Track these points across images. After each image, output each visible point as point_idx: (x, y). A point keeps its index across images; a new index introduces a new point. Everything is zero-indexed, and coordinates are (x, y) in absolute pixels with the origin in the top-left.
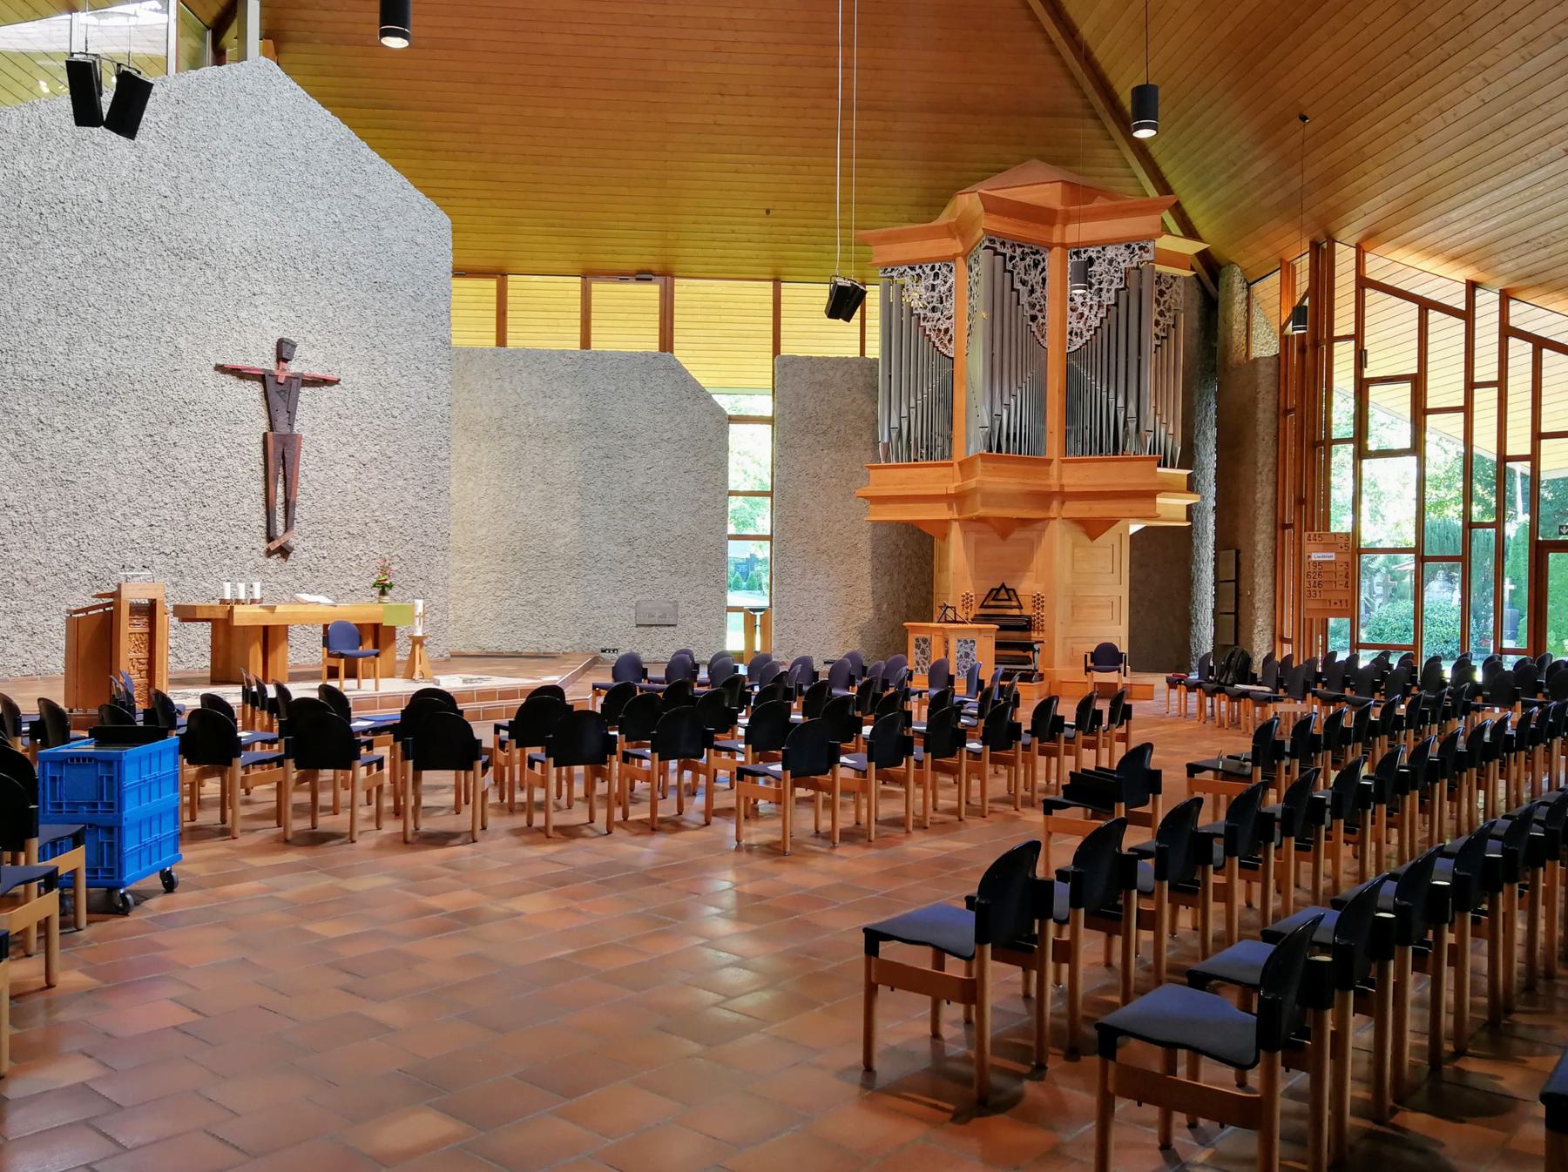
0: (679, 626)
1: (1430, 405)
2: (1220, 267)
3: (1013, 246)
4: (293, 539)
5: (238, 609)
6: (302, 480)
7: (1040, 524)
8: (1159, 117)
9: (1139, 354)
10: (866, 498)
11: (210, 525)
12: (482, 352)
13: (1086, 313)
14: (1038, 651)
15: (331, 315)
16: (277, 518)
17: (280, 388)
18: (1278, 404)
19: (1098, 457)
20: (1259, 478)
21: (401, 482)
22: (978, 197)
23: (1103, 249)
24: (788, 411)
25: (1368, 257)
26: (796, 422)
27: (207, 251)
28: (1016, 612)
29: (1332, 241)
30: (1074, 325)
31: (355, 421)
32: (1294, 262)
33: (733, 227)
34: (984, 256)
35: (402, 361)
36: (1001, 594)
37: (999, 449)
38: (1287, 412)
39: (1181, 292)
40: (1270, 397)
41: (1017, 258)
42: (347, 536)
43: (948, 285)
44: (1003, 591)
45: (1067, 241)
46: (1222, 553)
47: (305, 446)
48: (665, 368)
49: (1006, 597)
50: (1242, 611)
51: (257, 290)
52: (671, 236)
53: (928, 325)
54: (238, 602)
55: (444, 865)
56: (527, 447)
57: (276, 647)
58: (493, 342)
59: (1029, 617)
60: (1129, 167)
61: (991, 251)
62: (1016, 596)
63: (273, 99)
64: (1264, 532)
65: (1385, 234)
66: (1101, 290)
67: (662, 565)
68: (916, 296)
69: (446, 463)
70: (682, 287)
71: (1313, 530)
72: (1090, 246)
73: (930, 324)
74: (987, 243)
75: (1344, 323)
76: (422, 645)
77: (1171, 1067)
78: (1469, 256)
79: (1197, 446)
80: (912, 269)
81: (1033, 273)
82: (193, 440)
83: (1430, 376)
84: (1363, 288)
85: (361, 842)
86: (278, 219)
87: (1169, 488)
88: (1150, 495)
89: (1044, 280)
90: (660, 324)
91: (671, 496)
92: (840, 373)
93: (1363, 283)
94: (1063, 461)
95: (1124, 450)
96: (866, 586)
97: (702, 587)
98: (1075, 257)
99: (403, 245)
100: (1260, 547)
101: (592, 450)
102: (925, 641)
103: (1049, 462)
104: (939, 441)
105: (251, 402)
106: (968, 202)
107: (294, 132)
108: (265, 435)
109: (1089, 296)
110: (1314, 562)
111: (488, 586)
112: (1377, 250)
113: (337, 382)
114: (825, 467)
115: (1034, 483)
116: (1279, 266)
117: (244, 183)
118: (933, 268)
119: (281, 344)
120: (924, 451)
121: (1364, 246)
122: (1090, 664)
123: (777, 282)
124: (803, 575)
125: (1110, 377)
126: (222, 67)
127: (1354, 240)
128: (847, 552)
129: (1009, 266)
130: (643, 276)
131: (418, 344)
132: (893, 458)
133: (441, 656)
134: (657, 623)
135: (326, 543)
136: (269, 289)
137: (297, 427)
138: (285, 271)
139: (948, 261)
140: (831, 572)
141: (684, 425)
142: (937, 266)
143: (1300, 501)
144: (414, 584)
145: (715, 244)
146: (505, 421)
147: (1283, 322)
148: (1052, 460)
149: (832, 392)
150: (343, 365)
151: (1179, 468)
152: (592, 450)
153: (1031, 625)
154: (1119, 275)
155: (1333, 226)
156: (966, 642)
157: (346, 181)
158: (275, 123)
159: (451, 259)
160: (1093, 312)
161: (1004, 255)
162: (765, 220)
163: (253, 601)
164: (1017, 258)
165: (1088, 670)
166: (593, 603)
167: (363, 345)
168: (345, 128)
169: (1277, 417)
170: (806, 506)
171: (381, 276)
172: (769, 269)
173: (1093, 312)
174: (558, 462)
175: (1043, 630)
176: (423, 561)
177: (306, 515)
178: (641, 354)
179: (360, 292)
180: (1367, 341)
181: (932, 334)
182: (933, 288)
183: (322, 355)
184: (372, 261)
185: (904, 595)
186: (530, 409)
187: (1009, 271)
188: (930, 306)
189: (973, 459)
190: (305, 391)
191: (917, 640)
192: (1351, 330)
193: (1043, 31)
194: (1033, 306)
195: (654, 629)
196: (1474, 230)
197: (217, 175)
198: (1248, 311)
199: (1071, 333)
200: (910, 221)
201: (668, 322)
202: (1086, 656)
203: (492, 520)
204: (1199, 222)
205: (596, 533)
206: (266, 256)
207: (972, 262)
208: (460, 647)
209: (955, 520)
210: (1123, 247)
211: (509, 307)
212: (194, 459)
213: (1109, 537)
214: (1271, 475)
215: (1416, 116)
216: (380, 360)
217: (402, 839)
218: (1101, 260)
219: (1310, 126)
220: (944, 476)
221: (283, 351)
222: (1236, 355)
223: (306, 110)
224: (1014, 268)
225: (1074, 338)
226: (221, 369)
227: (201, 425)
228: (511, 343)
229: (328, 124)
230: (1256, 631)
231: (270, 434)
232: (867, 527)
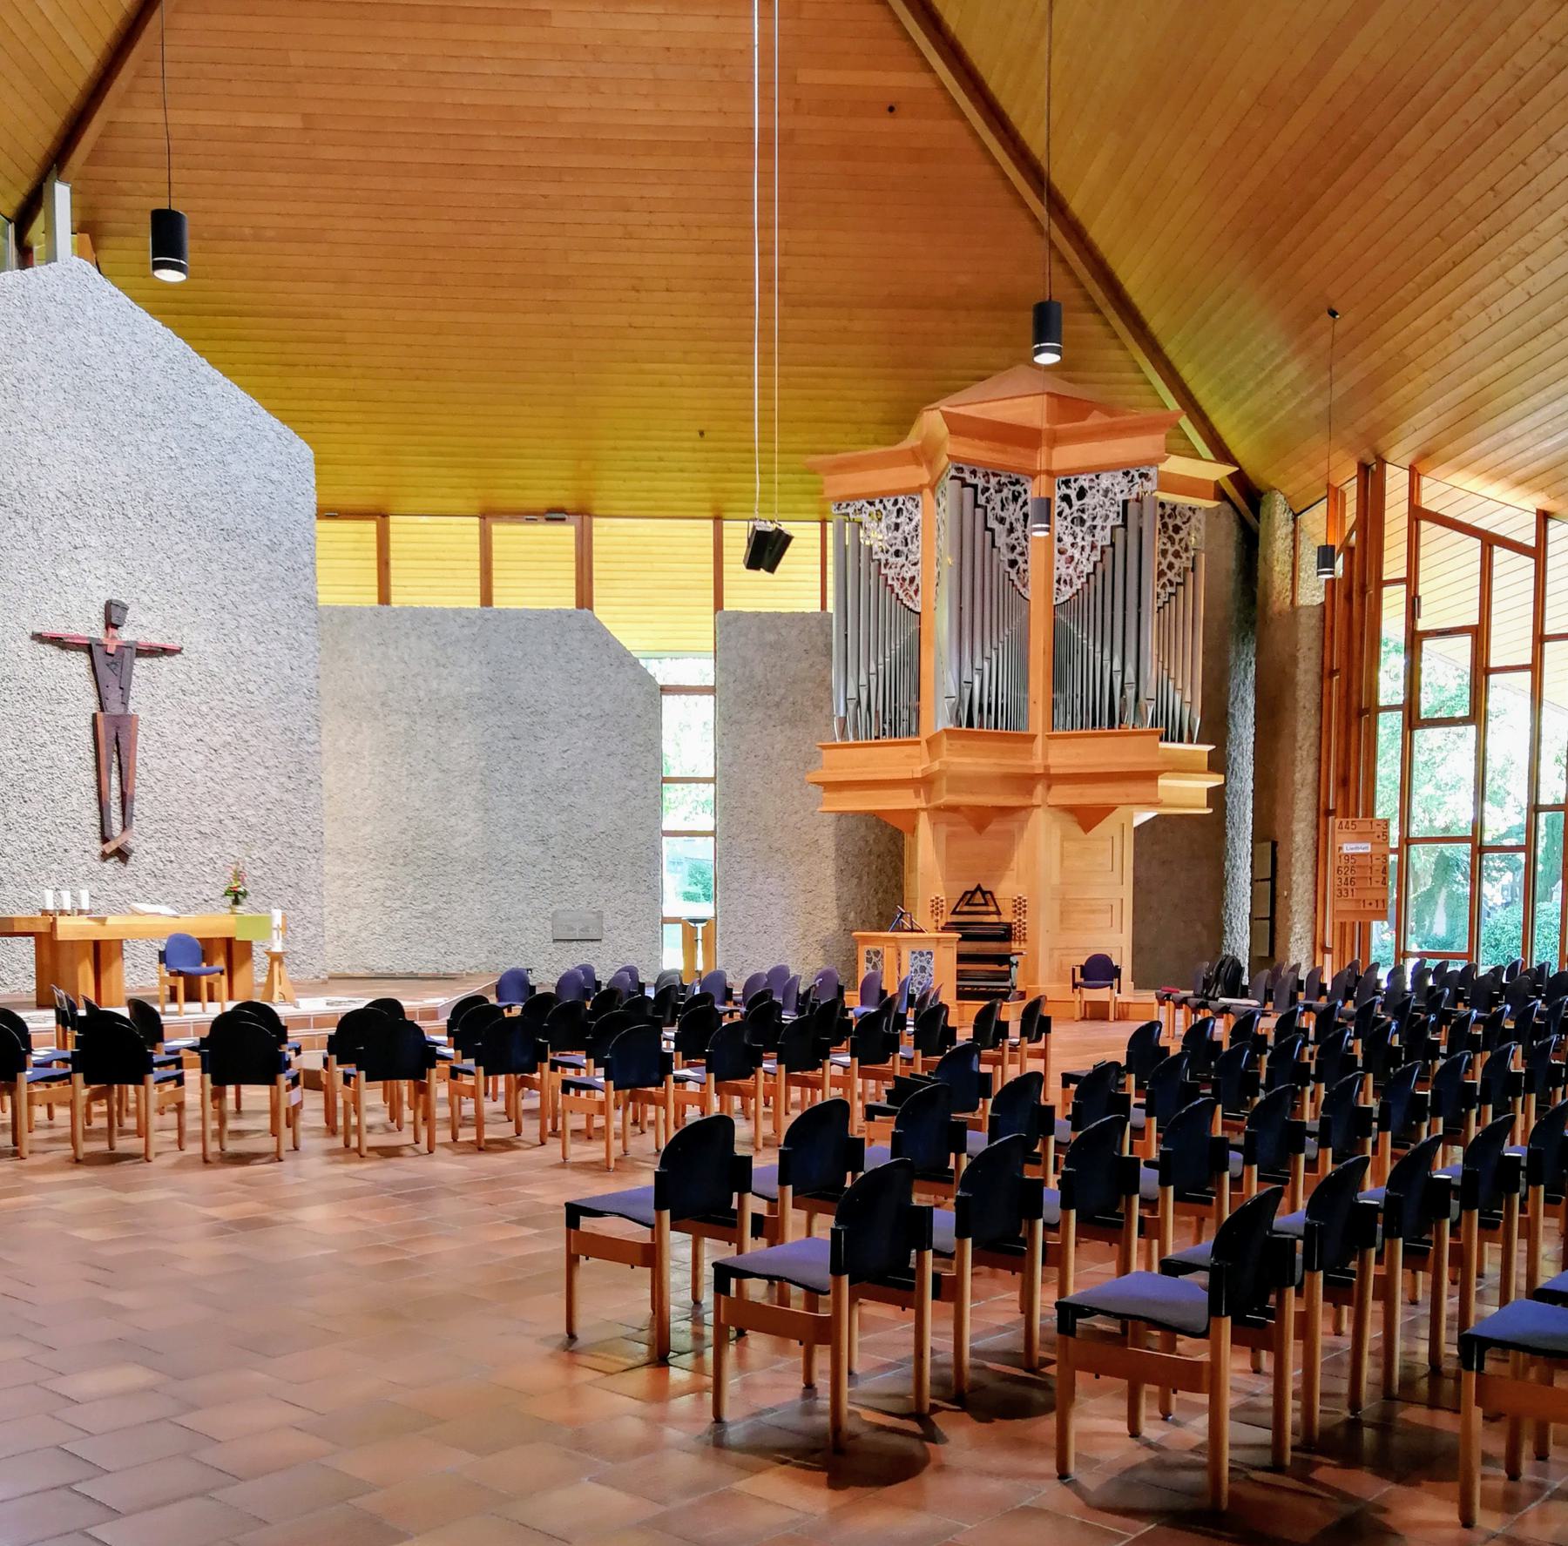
1: (1493, 664)
2: (1261, 494)
3: (986, 475)
4: (133, 840)
5: (62, 922)
6: (140, 770)
7: (1024, 812)
8: (1063, 339)
9: (1113, 610)
10: (818, 783)
11: (33, 823)
12: (360, 612)
13: (1077, 556)
14: (1017, 964)
15: (169, 570)
16: (113, 815)
17: (110, 659)
18: (1323, 663)
19: (1090, 731)
20: (1298, 753)
21: (261, 771)
22: (940, 414)
23: (1097, 477)
25: (1425, 481)
26: (743, 693)
27: (17, 496)
28: (994, 918)
29: (1382, 462)
30: (1063, 570)
31: (202, 697)
32: (1344, 488)
33: (662, 454)
34: (951, 487)
35: (258, 625)
36: (977, 896)
37: (970, 724)
38: (1332, 673)
39: (1202, 527)
41: (992, 491)
42: (198, 836)
43: (914, 523)
44: (979, 894)
45: (1055, 466)
46: (1257, 846)
47: (142, 729)
49: (982, 901)
50: (1278, 915)
51: (78, 542)
52: (585, 465)
54: (62, 913)
55: (237, 1182)
56: (417, 728)
57: (110, 964)
58: (375, 598)
59: (1010, 925)
60: (1140, 370)
61: (958, 482)
62: (994, 899)
63: (89, 308)
64: (1303, 820)
65: (1442, 452)
66: (1095, 527)
67: (582, 867)
68: (877, 536)
69: (316, 747)
70: (601, 526)
71: (1357, 816)
72: (1082, 473)
73: (893, 571)
74: (953, 473)
75: (1394, 564)
76: (281, 963)
77: (784, 1300)
78: (1537, 481)
79: (1233, 715)
80: (871, 504)
81: (1011, 507)
82: (9, 724)
83: (1494, 631)
84: (1417, 520)
85: (157, 1162)
86: (101, 456)
87: (1182, 768)
88: (1151, 776)
90: (577, 574)
91: (592, 784)
92: (794, 632)
93: (1417, 514)
94: (1050, 737)
96: (829, 891)
98: (1063, 487)
99: (255, 483)
101: (496, 729)
102: (877, 953)
103: (1034, 737)
104: (905, 714)
105: (76, 677)
106: (932, 421)
107: (117, 348)
108: (94, 716)
111: (375, 895)
113: (179, 651)
115: (1014, 763)
117: (58, 413)
118: (896, 503)
119: (109, 605)
120: (887, 727)
121: (1419, 467)
122: (1079, 979)
123: (718, 519)
124: (753, 878)
125: (1104, 635)
126: (26, 272)
127: (1406, 461)
128: (806, 849)
129: (982, 500)
130: (555, 515)
131: (277, 604)
132: (851, 735)
133: (317, 977)
135: (173, 843)
136: (93, 541)
137: (132, 705)
138: (111, 518)
139: (913, 492)
140: (787, 875)
142: (901, 500)
143: (1344, 782)
144: (279, 892)
146: (391, 695)
148: (1034, 737)
150: (186, 630)
151: (1197, 743)
152: (496, 729)
153: (1011, 934)
154: (1115, 508)
155: (1381, 443)
156: (921, 954)
157: (183, 407)
158: (94, 339)
159: (314, 499)
160: (1085, 555)
161: (975, 487)
162: (698, 445)
163: (81, 912)
164: (992, 491)
165: (1075, 986)
166: (501, 914)
167: (210, 606)
168: (180, 343)
169: (1321, 679)
170: (755, 794)
171: (228, 522)
173: (1085, 555)
174: (455, 745)
175: (1025, 940)
176: (291, 865)
177: (147, 812)
178: (553, 611)
179: (203, 542)
183: (159, 619)
184: (216, 504)
185: (875, 901)
186: (420, 681)
187: (979, 506)
188: (892, 550)
189: (938, 735)
190: (141, 663)
191: (868, 952)
192: (1403, 574)
193: (1025, 206)
196: (1539, 448)
197: (25, 403)
199: (1058, 581)
200: (876, 442)
203: (378, 816)
204: (1232, 440)
205: (503, 829)
206: (88, 501)
207: (939, 495)
208: (344, 967)
209: (923, 809)
211: (392, 555)
212: (11, 746)
214: (1313, 750)
215: (1457, 312)
216: (231, 624)
217: (201, 1158)
218: (1094, 491)
219: (1342, 324)
220: (908, 756)
221: (113, 616)
222: (1278, 604)
223: (130, 321)
224: (988, 501)
226: (39, 638)
227: (18, 705)
228: (397, 599)
229: (158, 339)
230: (1292, 939)
231: (100, 715)
232: (830, 818)
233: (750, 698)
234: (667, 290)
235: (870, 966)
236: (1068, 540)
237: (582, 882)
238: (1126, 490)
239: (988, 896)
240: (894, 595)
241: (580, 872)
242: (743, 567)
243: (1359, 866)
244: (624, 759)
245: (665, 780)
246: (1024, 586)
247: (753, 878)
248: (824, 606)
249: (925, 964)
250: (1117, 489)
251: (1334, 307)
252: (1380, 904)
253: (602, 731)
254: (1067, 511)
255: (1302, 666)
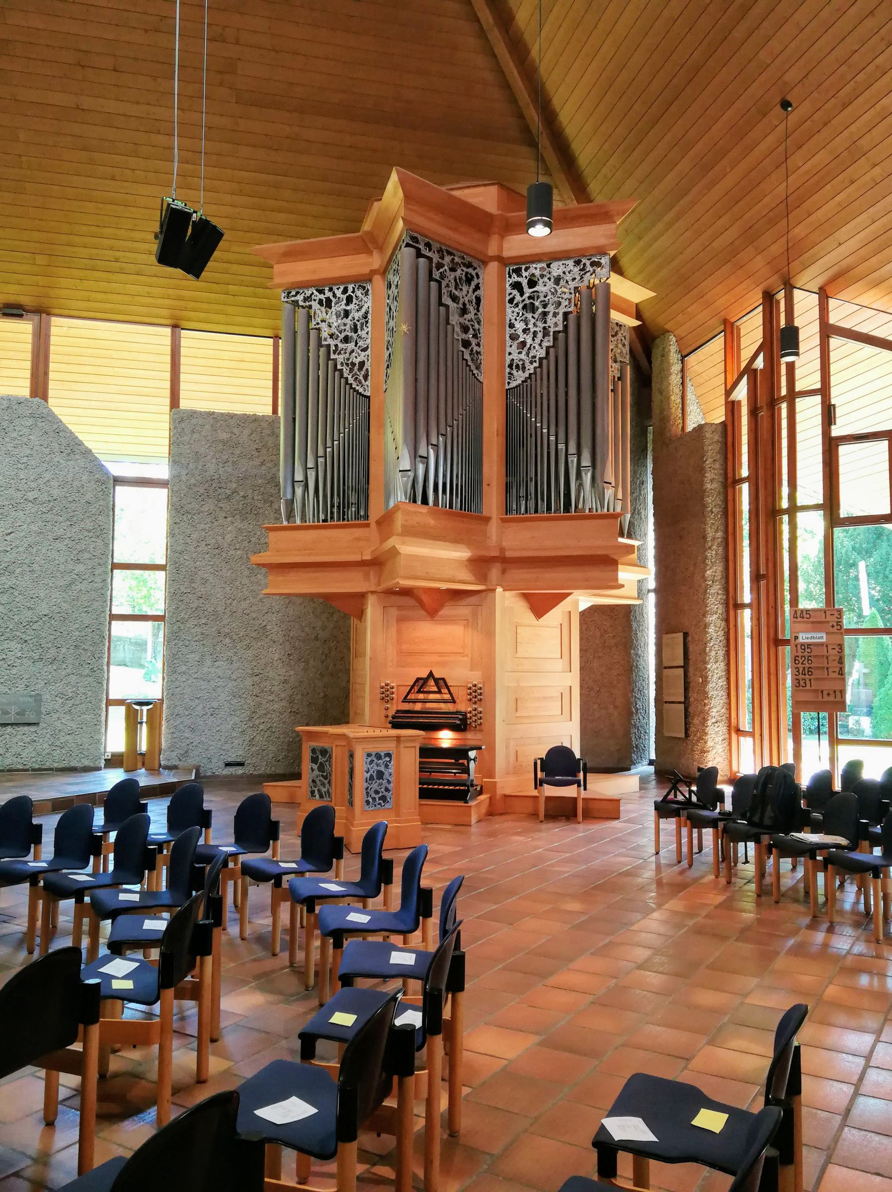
0: (42, 725)
2: (654, 338)
3: (440, 251)
10: (264, 565)
13: (529, 341)
23: (549, 266)
24: (184, 472)
25: (832, 303)
28: (450, 707)
29: (789, 287)
30: (515, 356)
32: (738, 323)
33: (118, 254)
40: (717, 465)
43: (363, 310)
44: (432, 682)
45: (506, 254)
46: (666, 638)
48: (32, 416)
49: (435, 689)
53: (340, 358)
62: (448, 687)
72: (533, 262)
80: (321, 292)
89: (478, 300)
91: (36, 567)
92: (247, 432)
93: (827, 331)
95: (576, 507)
97: (74, 677)
98: (514, 275)
100: (711, 630)
102: (324, 752)
103: (487, 520)
104: (353, 499)
109: (533, 321)
110: (802, 645)
112: (843, 295)
114: (229, 537)
116: (722, 328)
118: (345, 291)
124: (200, 662)
129: (436, 275)
134: (13, 721)
139: (363, 281)
140: (234, 658)
141: (54, 483)
145: (96, 274)
147: (729, 387)
149: (237, 452)
153: (465, 725)
156: (378, 757)
160: (538, 340)
161: (430, 259)
170: (205, 581)
172: (165, 312)
173: (538, 340)
180: (834, 392)
181: (344, 368)
182: (347, 314)
187: (436, 281)
188: (342, 336)
191: (313, 751)
194: (465, 329)
195: (9, 729)
198: (683, 384)
199: (510, 366)
201: (41, 366)
202: (535, 764)
209: (373, 592)
210: (571, 263)
213: (556, 615)
218: (546, 279)
219: (794, 117)
220: (358, 539)
225: (514, 372)
230: (709, 723)
233: (202, 491)
234: (115, 70)
235: (315, 767)
236: (520, 326)
237: (22, 665)
238: (578, 278)
239: (441, 683)
240: (343, 380)
241: (19, 654)
242: (153, 259)
243: (815, 656)
244: (71, 544)
245: (116, 566)
246: (478, 368)
247: (200, 662)
248: (275, 411)
249: (382, 768)
250: (569, 277)
251: (789, 98)
252: (838, 694)
253: (49, 516)
254: (518, 298)
255: (709, 475)
